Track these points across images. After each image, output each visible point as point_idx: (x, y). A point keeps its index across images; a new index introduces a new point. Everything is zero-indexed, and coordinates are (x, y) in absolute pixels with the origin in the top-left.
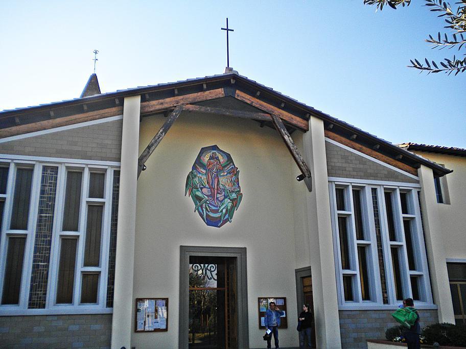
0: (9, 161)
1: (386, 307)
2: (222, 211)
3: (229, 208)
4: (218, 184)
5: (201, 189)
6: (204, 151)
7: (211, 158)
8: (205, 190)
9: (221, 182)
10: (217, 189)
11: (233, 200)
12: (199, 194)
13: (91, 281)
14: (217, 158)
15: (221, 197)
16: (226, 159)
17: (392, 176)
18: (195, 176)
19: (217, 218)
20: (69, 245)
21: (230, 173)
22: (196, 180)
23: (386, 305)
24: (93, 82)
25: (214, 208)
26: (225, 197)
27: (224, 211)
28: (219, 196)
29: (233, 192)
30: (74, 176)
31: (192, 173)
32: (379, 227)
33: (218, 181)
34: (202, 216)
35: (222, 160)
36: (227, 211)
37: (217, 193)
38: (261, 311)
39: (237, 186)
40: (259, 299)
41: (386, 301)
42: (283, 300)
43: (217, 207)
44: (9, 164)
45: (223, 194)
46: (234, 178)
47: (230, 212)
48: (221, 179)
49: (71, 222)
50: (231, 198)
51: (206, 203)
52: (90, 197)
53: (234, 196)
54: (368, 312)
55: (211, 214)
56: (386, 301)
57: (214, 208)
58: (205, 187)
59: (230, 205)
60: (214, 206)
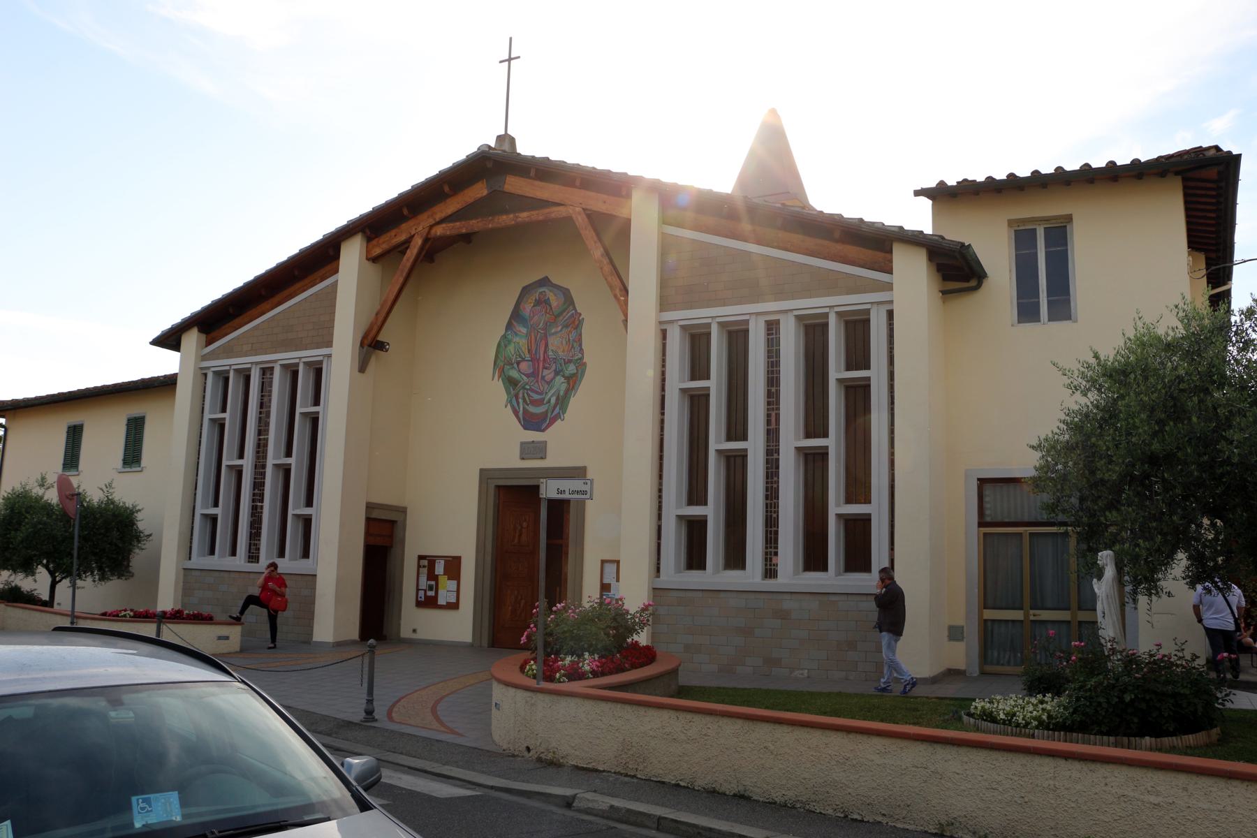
0: (827, 310)
1: (770, 584)
2: (549, 401)
3: (562, 393)
4: (545, 352)
5: (518, 363)
6: (526, 291)
7: (538, 302)
8: (524, 366)
9: (550, 347)
10: (544, 360)
11: (568, 378)
12: (514, 374)
13: (858, 530)
14: (547, 302)
15: (548, 374)
16: (563, 300)
17: (830, 284)
18: (510, 342)
19: (537, 415)
20: (814, 461)
21: (567, 326)
22: (511, 348)
23: (772, 581)
24: (774, 152)
25: (536, 397)
26: (557, 373)
27: (553, 400)
28: (546, 372)
29: (570, 361)
30: (814, 331)
31: (504, 337)
32: (769, 403)
33: (546, 345)
34: (516, 413)
35: (554, 303)
36: (558, 399)
37: (545, 368)
38: (455, 582)
39: (577, 348)
40: (603, 562)
41: (770, 572)
42: (607, 566)
43: (541, 394)
44: (709, 325)
45: (553, 367)
46: (573, 335)
47: (563, 402)
48: (551, 340)
49: (815, 424)
50: (567, 373)
51: (524, 388)
52: (848, 368)
53: (571, 369)
54: (722, 595)
55: (532, 409)
56: (770, 572)
57: (536, 397)
58: (524, 360)
59: (564, 387)
60: (536, 392)
